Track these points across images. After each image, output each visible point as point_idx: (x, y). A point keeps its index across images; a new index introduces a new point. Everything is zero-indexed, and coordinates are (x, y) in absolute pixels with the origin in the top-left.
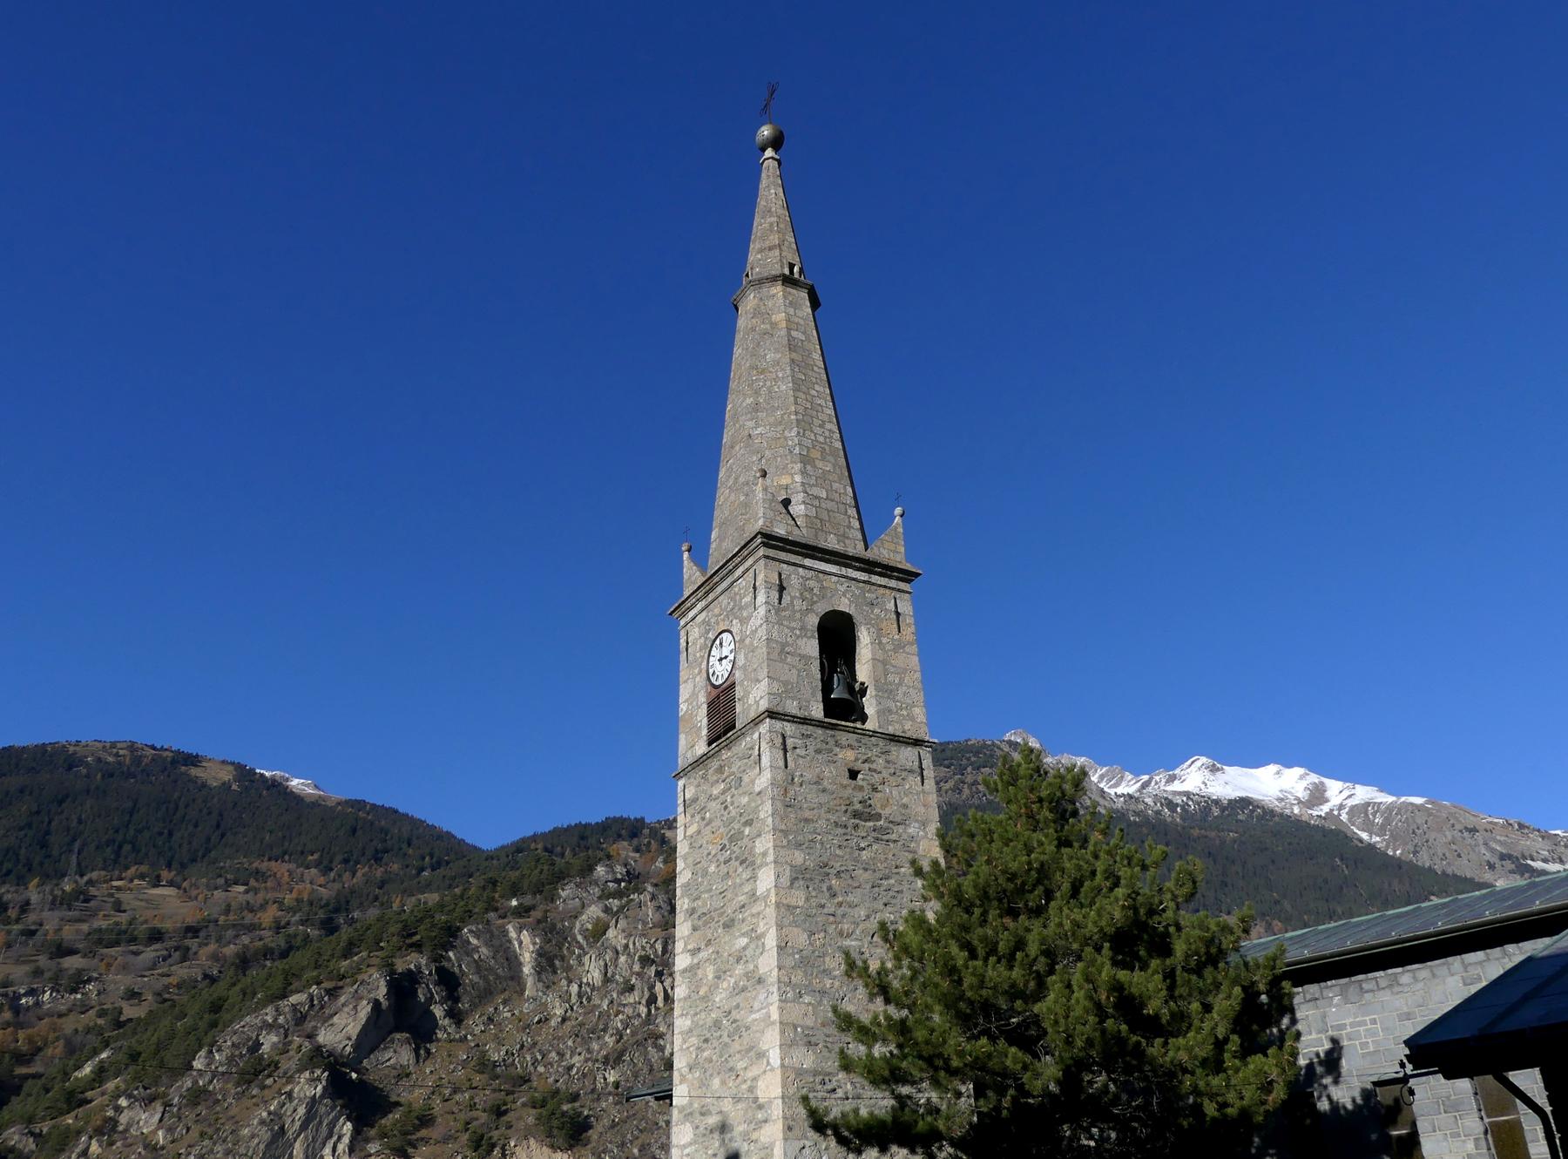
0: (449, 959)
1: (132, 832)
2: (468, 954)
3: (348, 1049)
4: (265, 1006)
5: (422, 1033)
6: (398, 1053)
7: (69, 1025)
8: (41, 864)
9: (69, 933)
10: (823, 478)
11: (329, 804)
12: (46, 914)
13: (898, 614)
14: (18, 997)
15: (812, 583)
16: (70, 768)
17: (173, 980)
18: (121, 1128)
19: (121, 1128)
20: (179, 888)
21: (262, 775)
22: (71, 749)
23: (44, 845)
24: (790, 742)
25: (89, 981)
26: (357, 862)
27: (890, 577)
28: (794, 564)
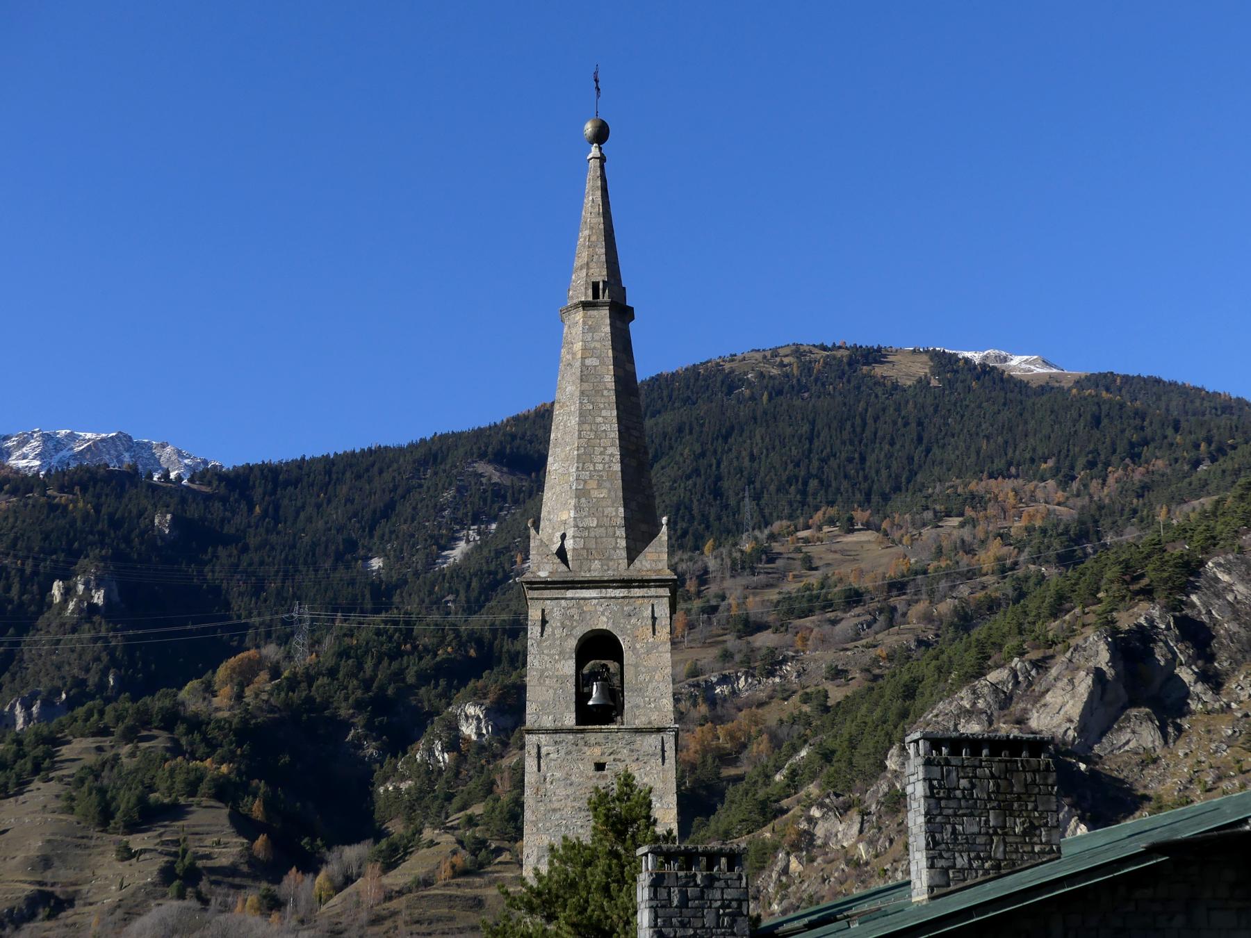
0: (1193, 606)
1: (815, 464)
2: (1218, 595)
3: (1071, 733)
4: (960, 688)
5: (1169, 708)
6: (1137, 735)
7: (772, 715)
8: (719, 518)
9: (754, 606)
10: (596, 509)
12: (728, 583)
13: (654, 619)
14: (710, 687)
15: (573, 611)
16: (730, 393)
17: (881, 651)
18: (819, 842)
19: (819, 842)
20: (878, 530)
21: (967, 360)
22: (727, 366)
23: (717, 493)
24: (544, 751)
25: (785, 661)
26: (1107, 464)
27: (649, 587)
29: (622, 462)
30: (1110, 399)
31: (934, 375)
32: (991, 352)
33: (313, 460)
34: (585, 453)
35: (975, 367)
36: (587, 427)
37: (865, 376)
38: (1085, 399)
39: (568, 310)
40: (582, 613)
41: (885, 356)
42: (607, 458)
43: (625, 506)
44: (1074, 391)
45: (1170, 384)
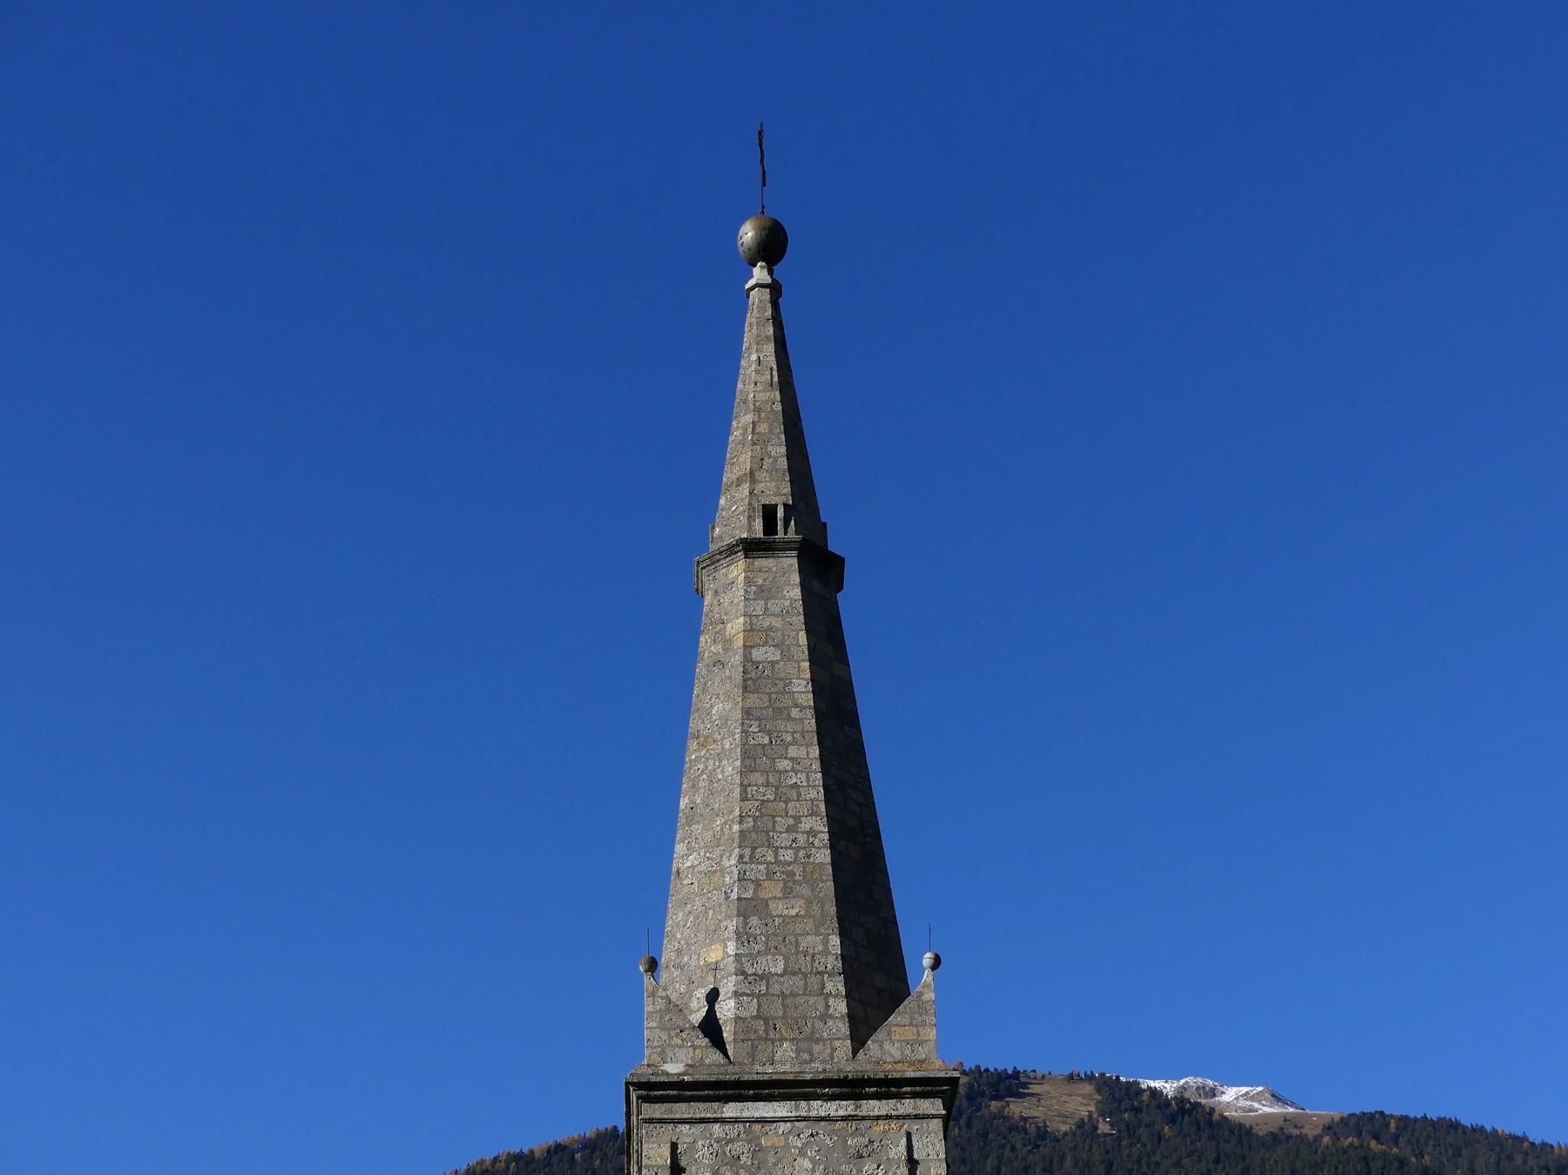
10: (782, 938)
11: (1310, 1132)
15: (738, 1147)
21: (1154, 1093)
27: (900, 1096)
28: (702, 1121)
29: (832, 847)
30: (1383, 1153)
31: (1103, 1114)
32: (1190, 1080)
34: (755, 829)
35: (1167, 1103)
36: (758, 778)
37: (994, 1117)
38: (1345, 1152)
39: (714, 560)
40: (757, 1151)
41: (1025, 1085)
42: (802, 839)
43: (844, 934)
44: (1326, 1139)
45: (1474, 1130)
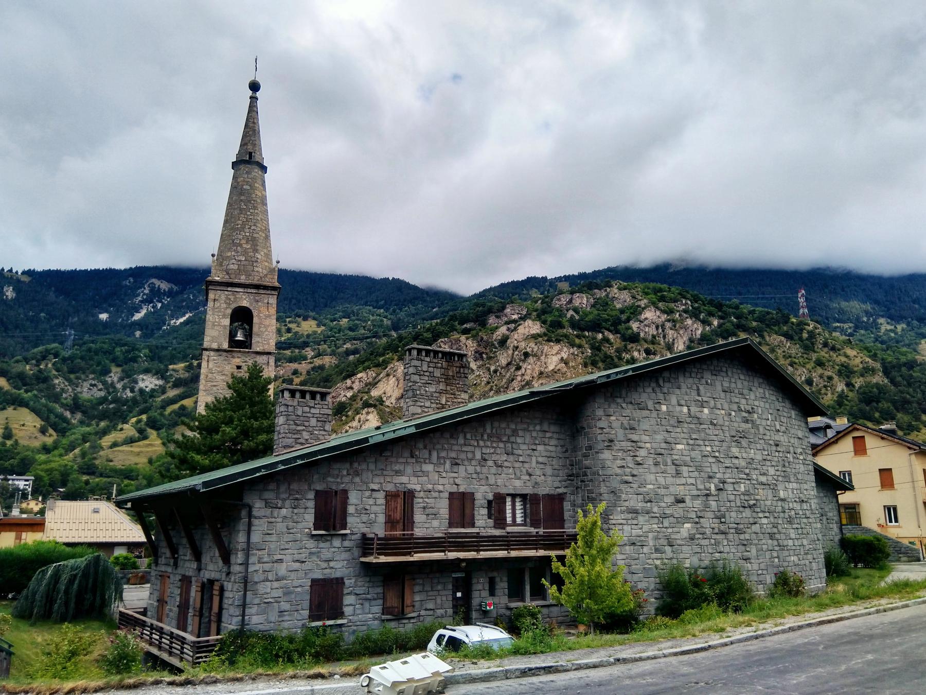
33: (80, 271)
